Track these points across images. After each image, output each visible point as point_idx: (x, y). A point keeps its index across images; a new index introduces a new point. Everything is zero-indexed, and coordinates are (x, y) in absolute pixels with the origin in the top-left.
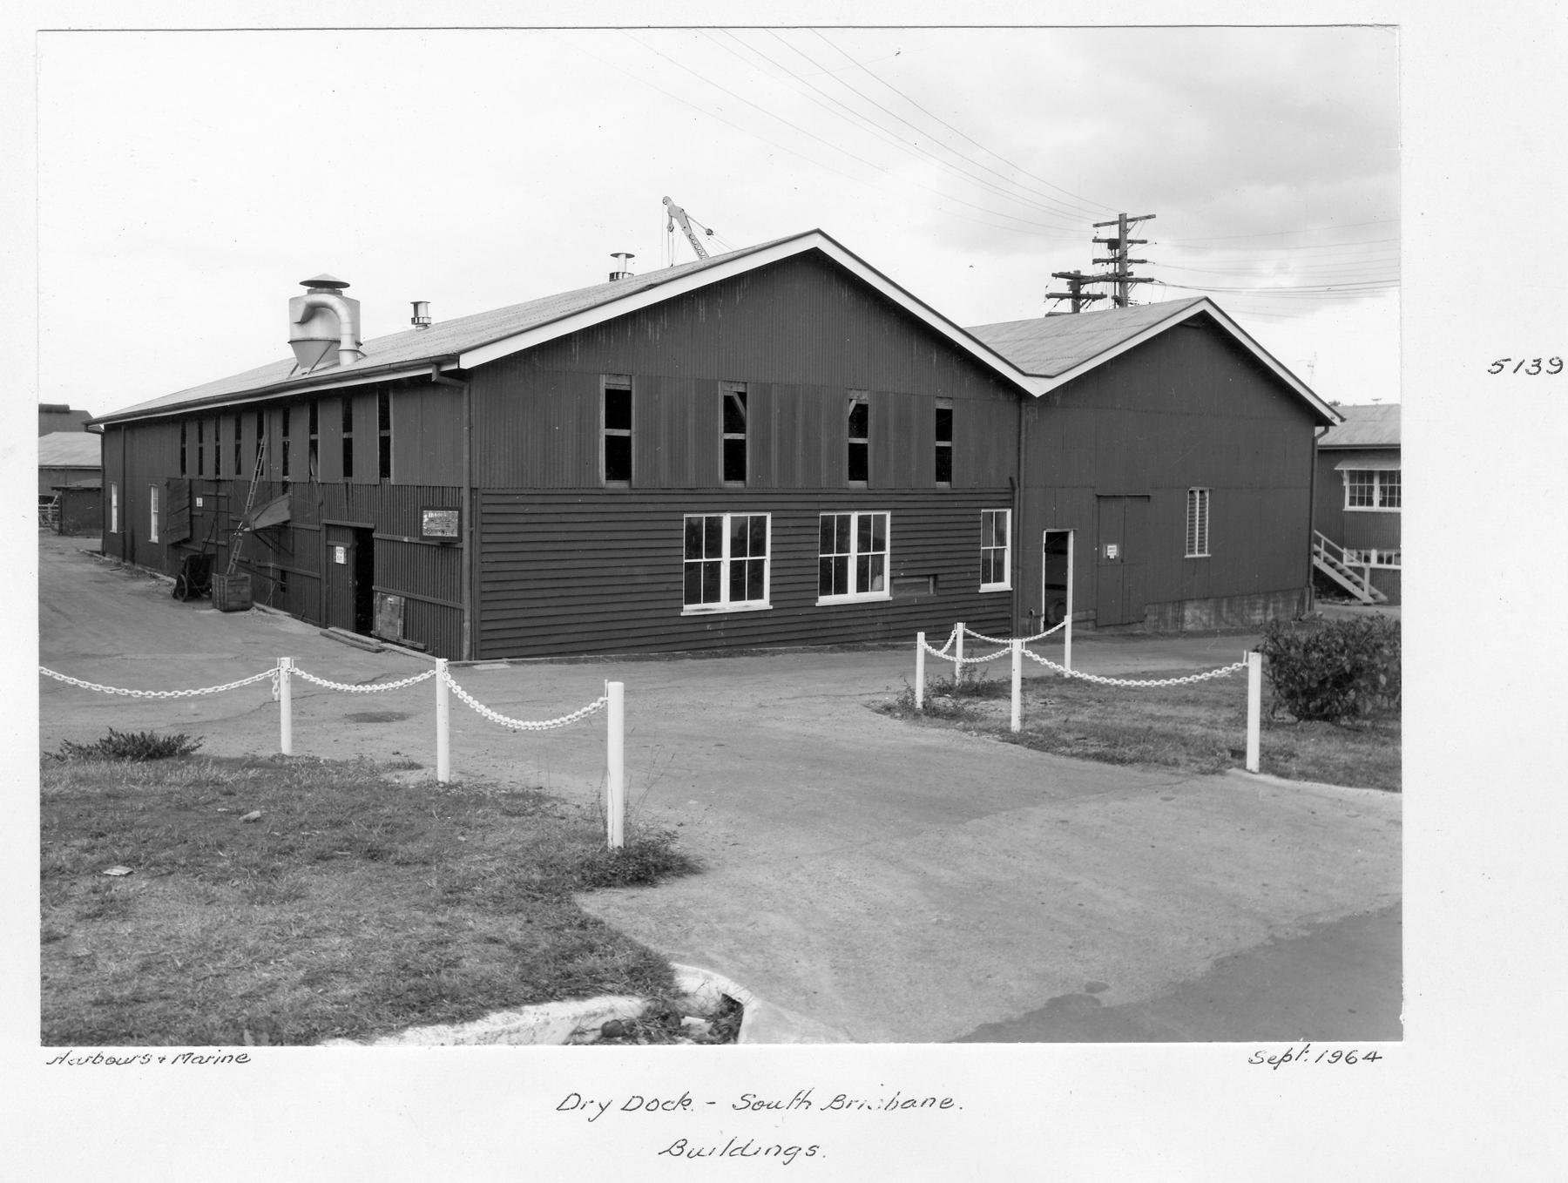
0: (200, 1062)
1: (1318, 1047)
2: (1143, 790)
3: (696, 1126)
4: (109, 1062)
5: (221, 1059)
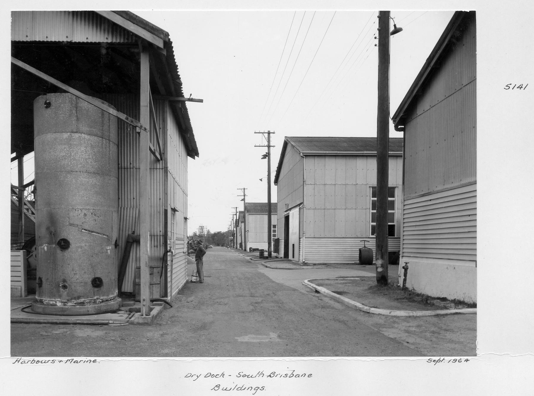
0: (77, 363)
1: (447, 358)
2: (109, 300)
3: (224, 382)
4: (212, 377)
5: (232, 389)
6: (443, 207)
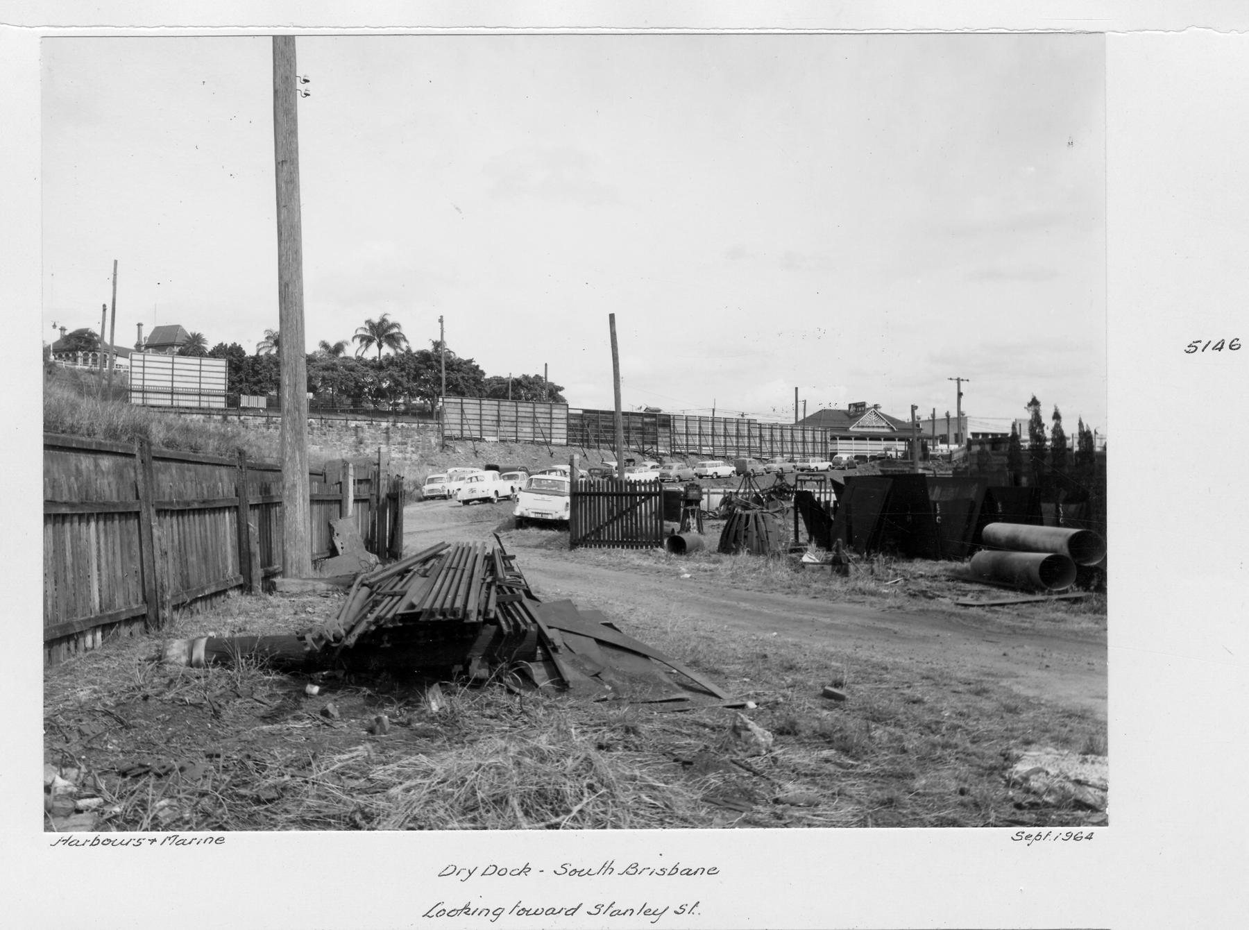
6: (422, 531)
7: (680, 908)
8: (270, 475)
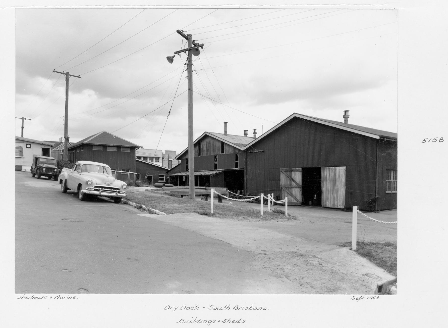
1: (367, 296)
7: (46, 297)
8: (347, 118)
